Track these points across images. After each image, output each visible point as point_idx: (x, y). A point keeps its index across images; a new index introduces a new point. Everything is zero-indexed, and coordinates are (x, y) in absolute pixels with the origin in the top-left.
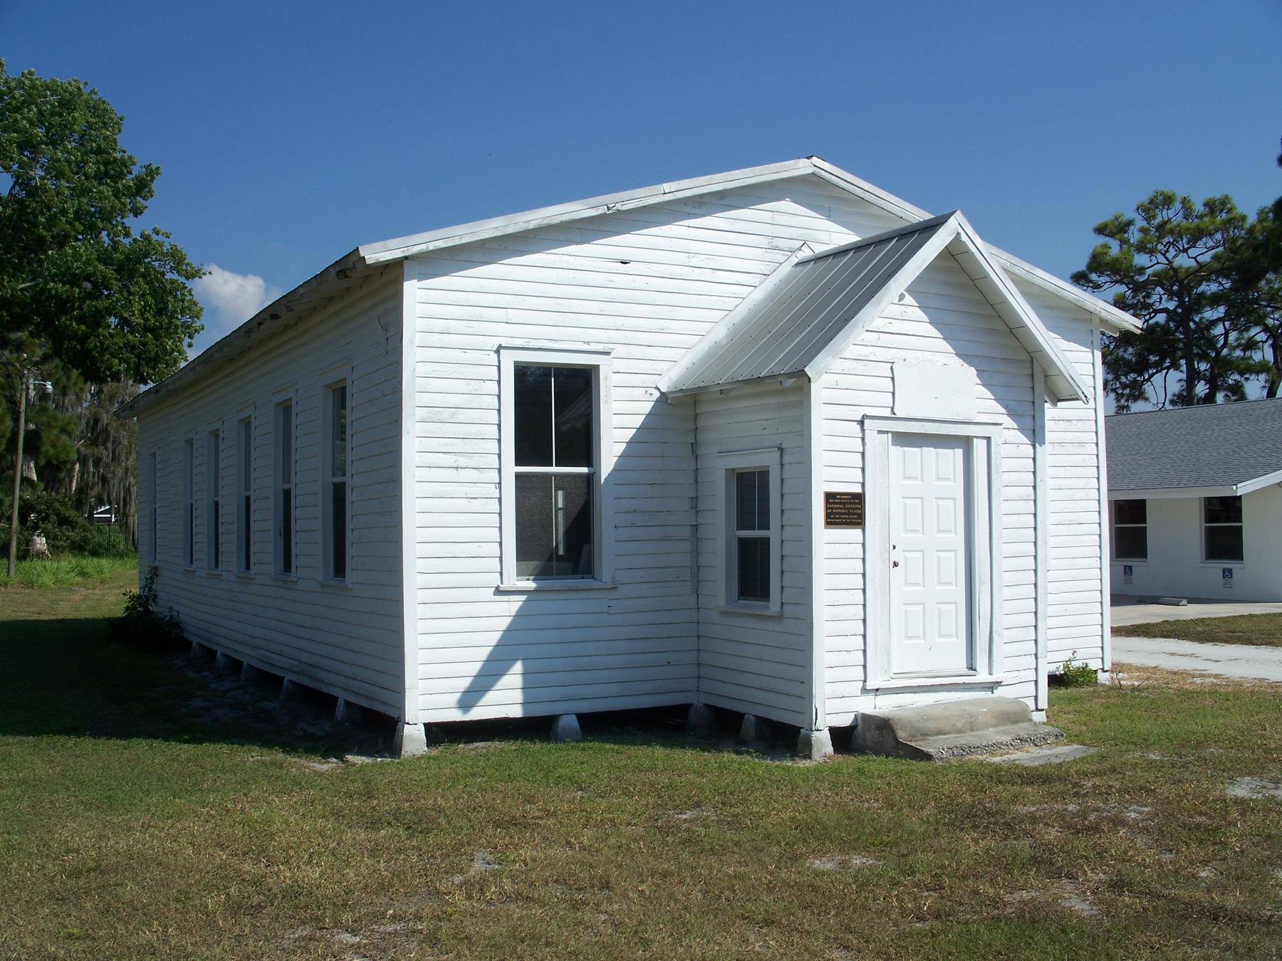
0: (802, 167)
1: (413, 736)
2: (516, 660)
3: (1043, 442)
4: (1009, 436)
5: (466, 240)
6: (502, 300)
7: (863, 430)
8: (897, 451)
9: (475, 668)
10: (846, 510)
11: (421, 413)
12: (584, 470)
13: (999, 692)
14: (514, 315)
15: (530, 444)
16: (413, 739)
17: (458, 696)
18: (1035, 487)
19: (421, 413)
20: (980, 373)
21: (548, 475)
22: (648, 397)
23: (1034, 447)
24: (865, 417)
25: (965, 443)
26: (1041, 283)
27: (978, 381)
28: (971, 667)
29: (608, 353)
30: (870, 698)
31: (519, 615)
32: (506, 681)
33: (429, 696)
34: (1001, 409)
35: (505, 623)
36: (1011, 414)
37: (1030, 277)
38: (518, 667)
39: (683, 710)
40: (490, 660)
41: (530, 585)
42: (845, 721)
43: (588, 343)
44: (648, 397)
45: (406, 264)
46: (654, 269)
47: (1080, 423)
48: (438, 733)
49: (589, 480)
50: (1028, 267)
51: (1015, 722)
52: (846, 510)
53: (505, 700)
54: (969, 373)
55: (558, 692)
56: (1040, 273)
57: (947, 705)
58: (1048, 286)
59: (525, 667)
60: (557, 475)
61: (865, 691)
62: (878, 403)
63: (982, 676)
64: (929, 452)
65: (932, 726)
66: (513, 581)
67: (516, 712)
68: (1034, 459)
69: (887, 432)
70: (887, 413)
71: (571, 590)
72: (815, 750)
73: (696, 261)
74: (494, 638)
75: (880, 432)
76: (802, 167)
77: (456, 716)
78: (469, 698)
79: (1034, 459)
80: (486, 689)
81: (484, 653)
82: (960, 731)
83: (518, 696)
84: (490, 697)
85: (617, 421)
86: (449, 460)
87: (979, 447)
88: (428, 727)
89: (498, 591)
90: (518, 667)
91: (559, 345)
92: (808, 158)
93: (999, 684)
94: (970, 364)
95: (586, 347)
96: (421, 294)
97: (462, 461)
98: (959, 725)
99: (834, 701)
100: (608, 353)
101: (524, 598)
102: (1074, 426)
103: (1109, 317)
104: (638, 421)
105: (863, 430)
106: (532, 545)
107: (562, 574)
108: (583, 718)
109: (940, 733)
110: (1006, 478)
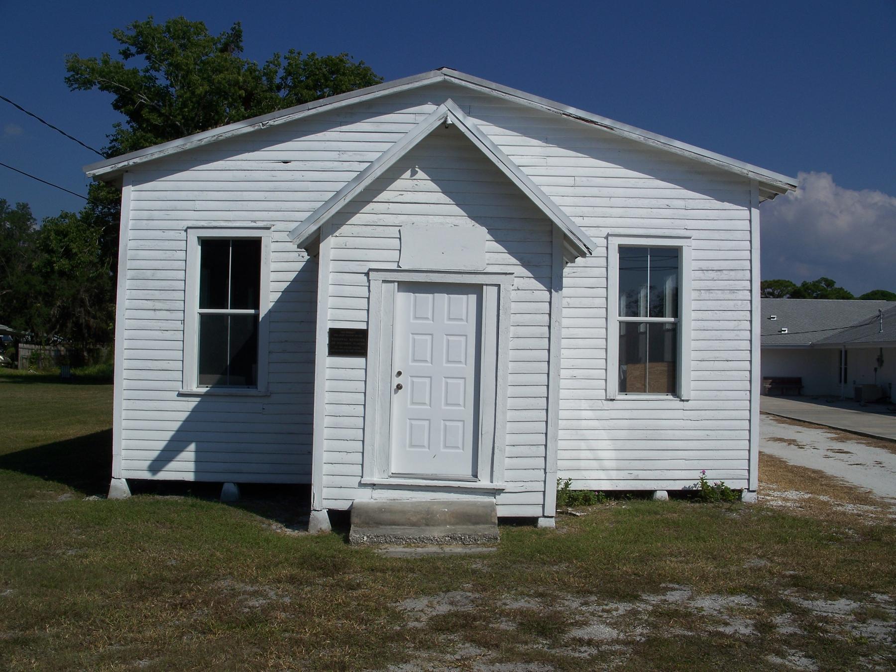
0: (434, 78)
1: (119, 486)
2: (192, 442)
3: (559, 288)
4: (521, 284)
5: (156, 156)
6: (191, 195)
7: (369, 281)
8: (403, 299)
9: (162, 445)
10: (349, 343)
11: (130, 274)
12: (252, 311)
13: (500, 498)
14: (198, 205)
15: (211, 293)
16: (116, 488)
17: (148, 463)
18: (549, 327)
19: (130, 274)
20: (490, 231)
21: (227, 315)
22: (300, 259)
23: (551, 293)
24: (370, 270)
25: (477, 289)
26: (679, 152)
27: (489, 237)
28: (475, 475)
29: (269, 228)
30: (368, 491)
31: (194, 411)
32: (184, 455)
33: (129, 460)
34: (514, 260)
35: (184, 416)
36: (525, 264)
37: (666, 148)
38: (192, 447)
39: (218, 486)
40: (173, 440)
41: (203, 390)
42: (343, 506)
43: (255, 221)
44: (300, 259)
45: (126, 177)
46: (309, 165)
47: (732, 273)
48: (136, 486)
49: (256, 316)
50: (663, 139)
51: (476, 523)
52: (349, 343)
53: (182, 468)
54: (482, 231)
55: (623, 474)
56: (678, 144)
57: (474, 504)
58: (686, 154)
59: (197, 446)
60: (234, 316)
61: (362, 485)
62: (386, 258)
63: (484, 482)
64: (443, 299)
65: (387, 517)
66: (194, 386)
67: (190, 477)
68: (550, 303)
69: (394, 282)
70: (394, 266)
71: (231, 396)
72: (311, 525)
73: (345, 157)
74: (176, 426)
75: (384, 281)
76: (434, 78)
77: (147, 476)
78: (157, 465)
79: (550, 303)
80: (170, 460)
81: (169, 435)
82: (413, 525)
83: (191, 466)
84: (172, 465)
85: (273, 276)
86: (149, 304)
87: (490, 294)
88: (130, 482)
89: (180, 395)
90: (192, 447)
91: (232, 222)
92: (439, 69)
93: (500, 491)
94: (482, 224)
95: (253, 225)
96: (133, 195)
97: (158, 305)
98: (414, 519)
99: (329, 492)
100: (269, 228)
101: (198, 399)
102: (725, 275)
103: (763, 179)
104: (292, 276)
105: (369, 281)
106: (209, 363)
107: (234, 384)
108: (241, 486)
109: (394, 523)
110: (514, 319)
